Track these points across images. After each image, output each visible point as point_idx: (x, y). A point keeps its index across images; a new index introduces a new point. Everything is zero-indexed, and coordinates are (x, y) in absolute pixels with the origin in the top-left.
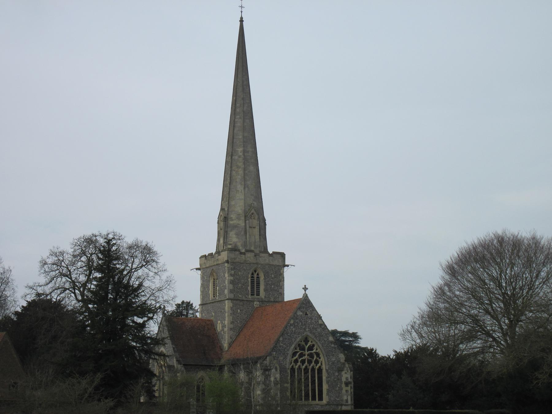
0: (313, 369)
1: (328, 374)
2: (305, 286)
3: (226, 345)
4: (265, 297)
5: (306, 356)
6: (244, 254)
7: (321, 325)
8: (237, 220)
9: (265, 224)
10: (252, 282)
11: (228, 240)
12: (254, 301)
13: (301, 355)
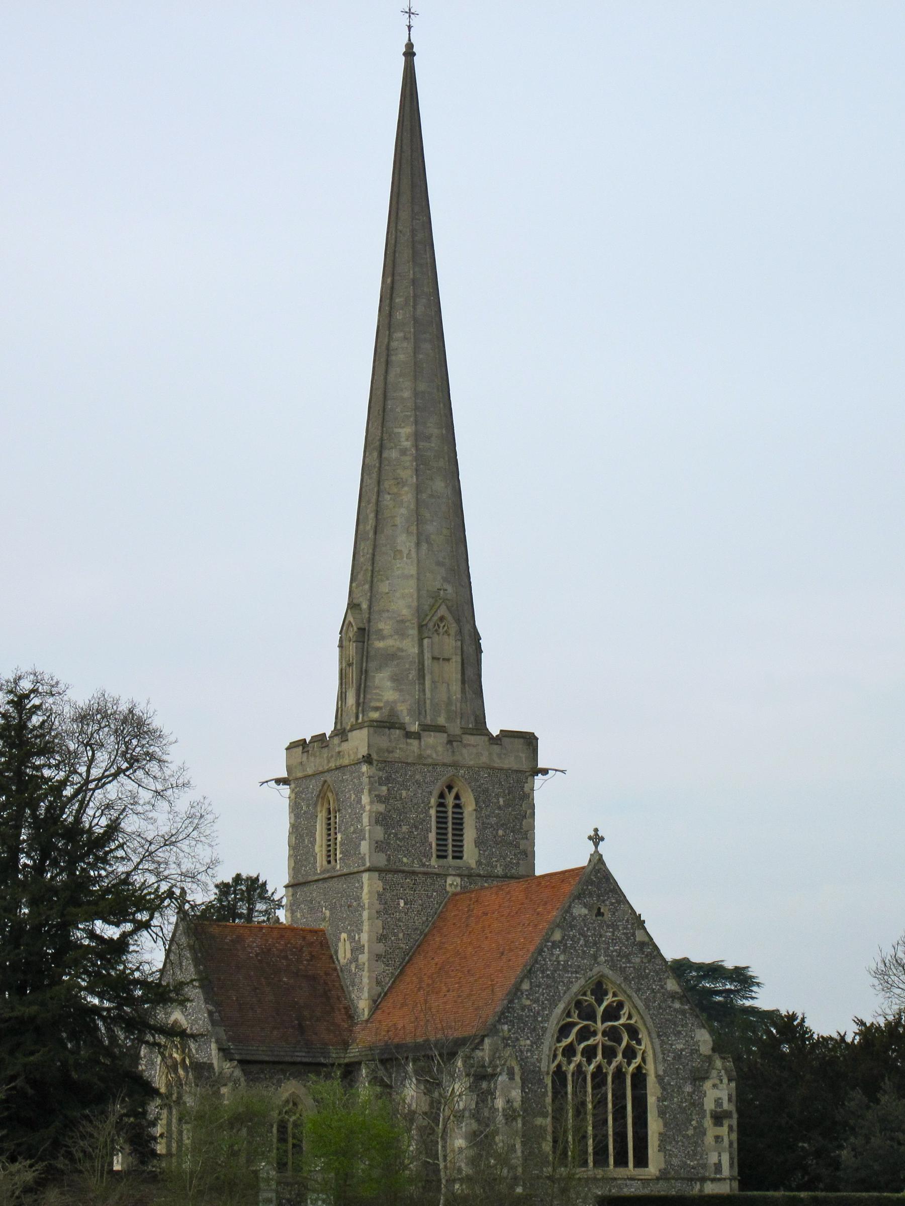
0: (619, 1075)
1: (664, 1089)
2: (596, 830)
3: (363, 1005)
4: (479, 863)
5: (599, 1037)
6: (417, 736)
7: (642, 945)
8: (396, 637)
9: (479, 650)
10: (441, 820)
11: (368, 696)
12: (446, 875)
13: (585, 1034)
